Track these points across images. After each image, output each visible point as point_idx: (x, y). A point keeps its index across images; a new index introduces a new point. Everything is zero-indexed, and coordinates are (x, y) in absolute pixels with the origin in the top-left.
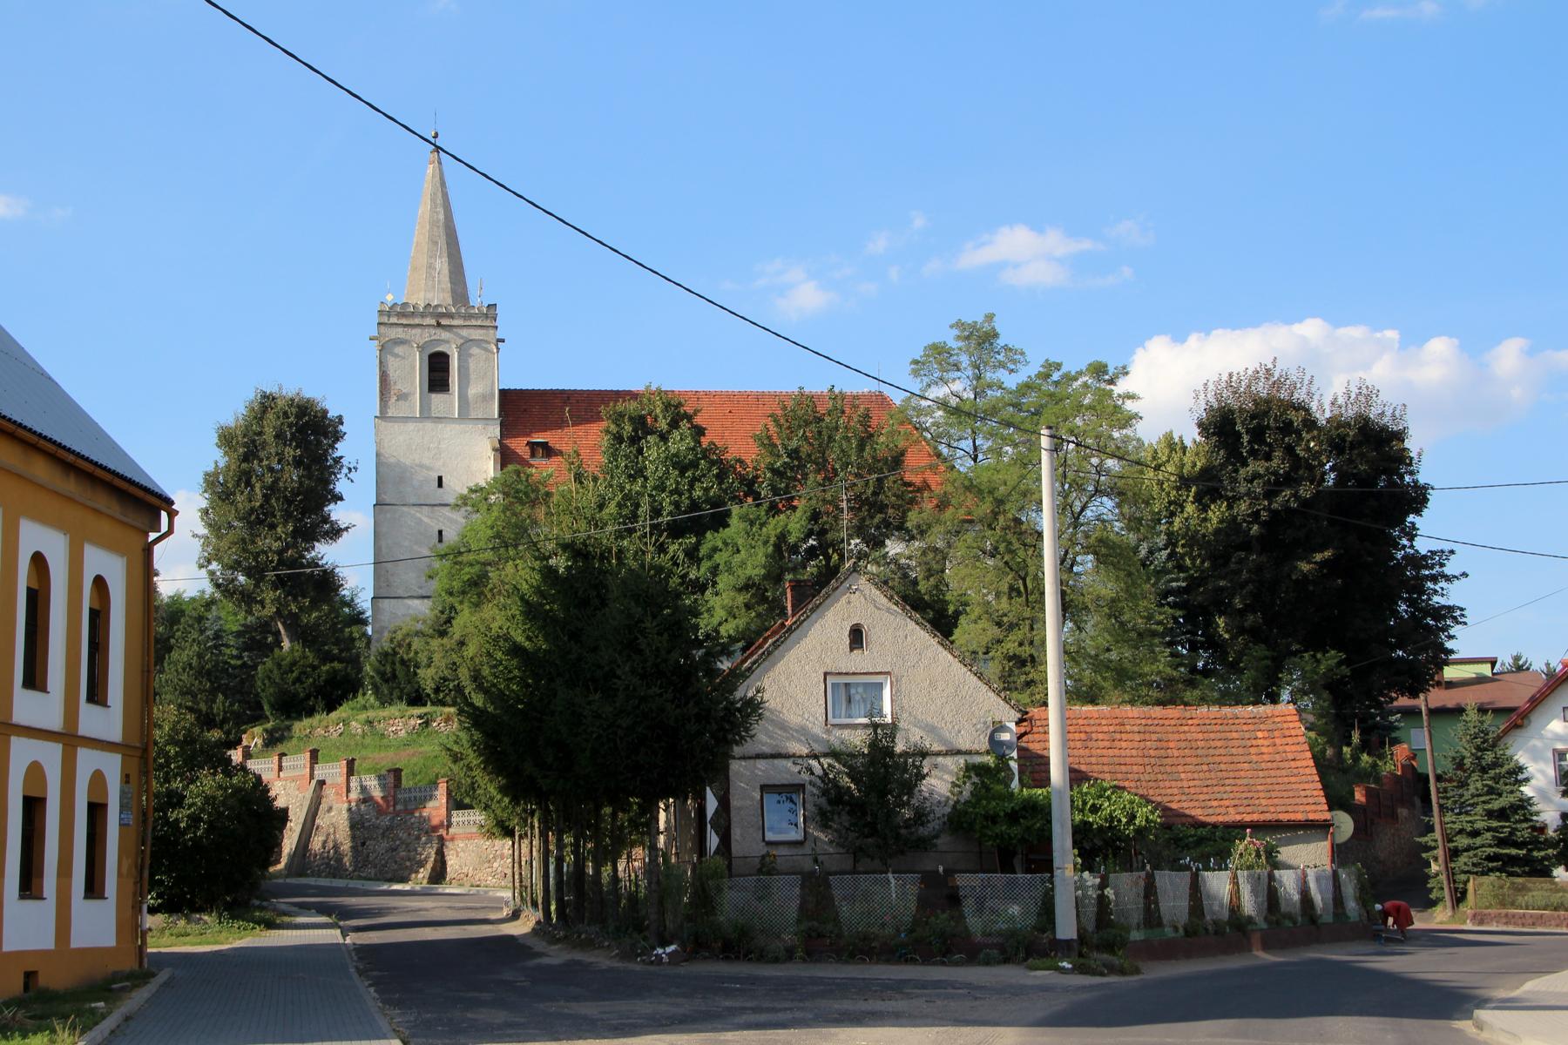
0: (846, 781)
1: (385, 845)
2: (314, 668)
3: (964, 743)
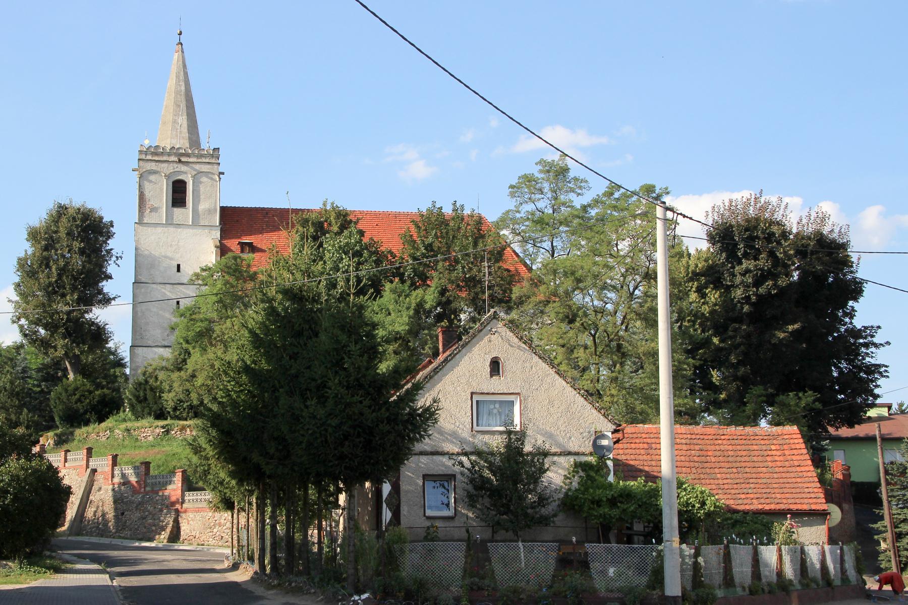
0: (487, 473)
1: (138, 515)
2: (90, 392)
3: (573, 447)
